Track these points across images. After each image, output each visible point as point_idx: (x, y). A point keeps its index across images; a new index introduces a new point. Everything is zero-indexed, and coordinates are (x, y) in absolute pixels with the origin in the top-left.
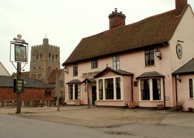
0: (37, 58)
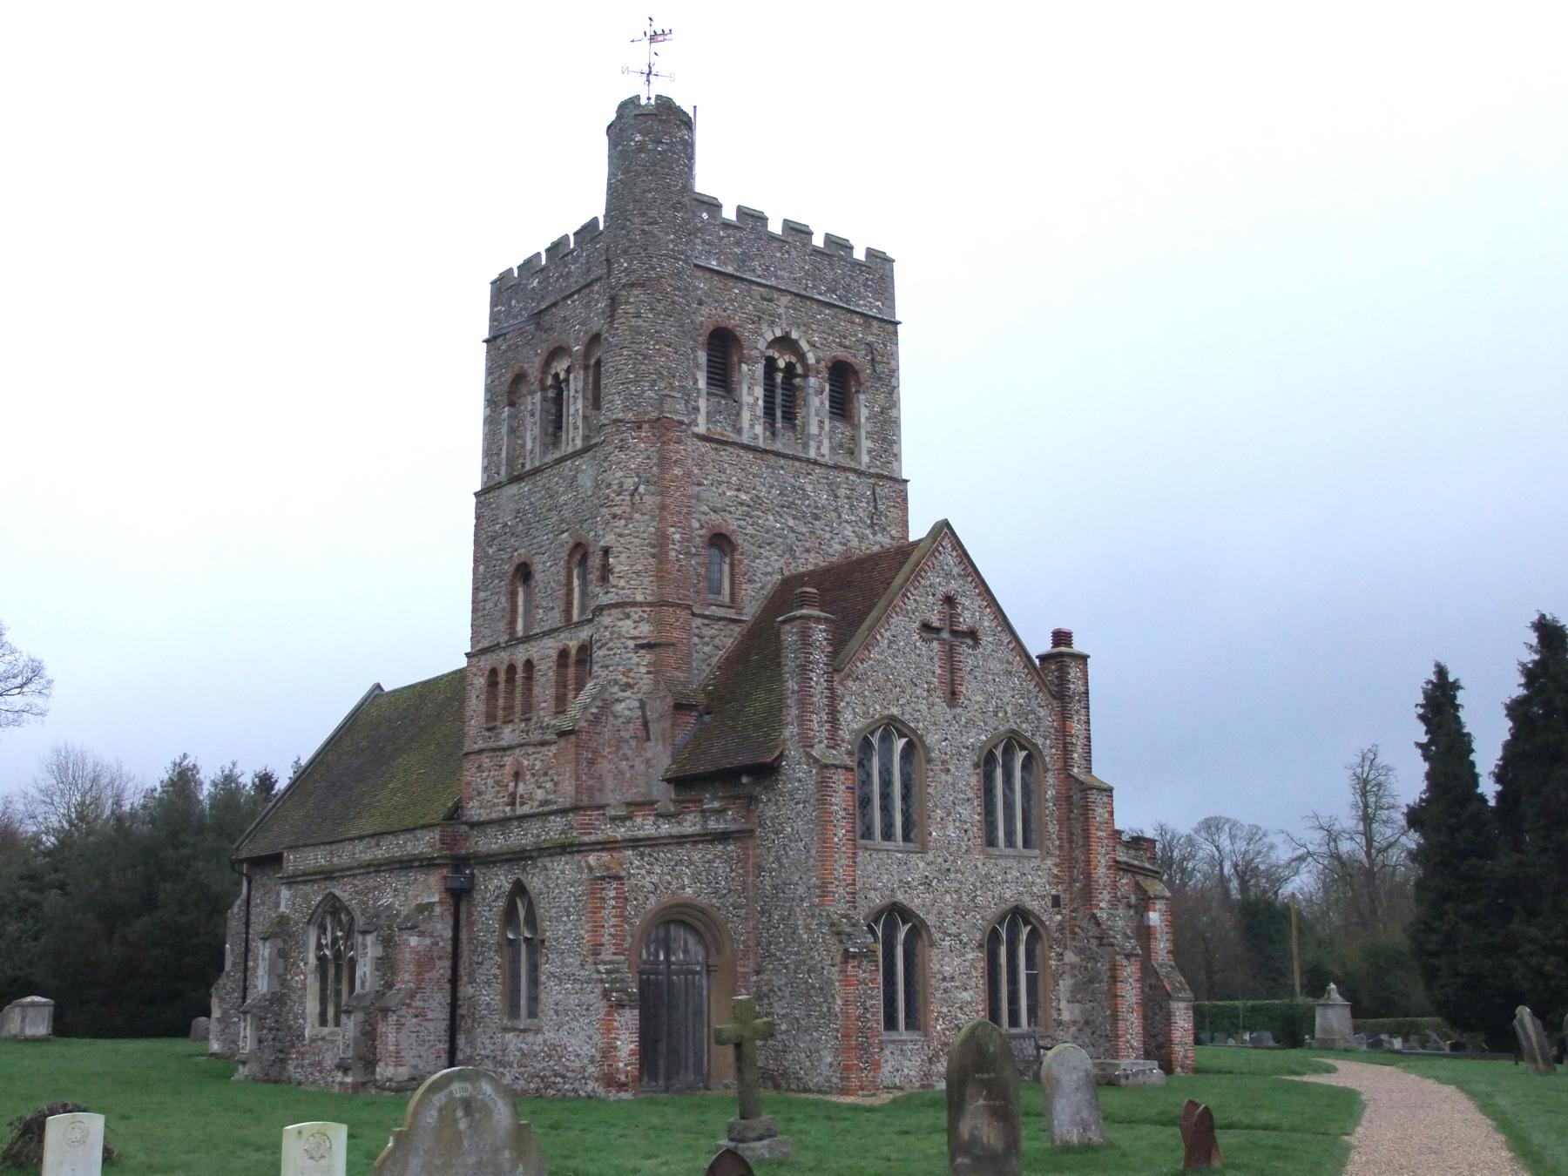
0: (555, 425)
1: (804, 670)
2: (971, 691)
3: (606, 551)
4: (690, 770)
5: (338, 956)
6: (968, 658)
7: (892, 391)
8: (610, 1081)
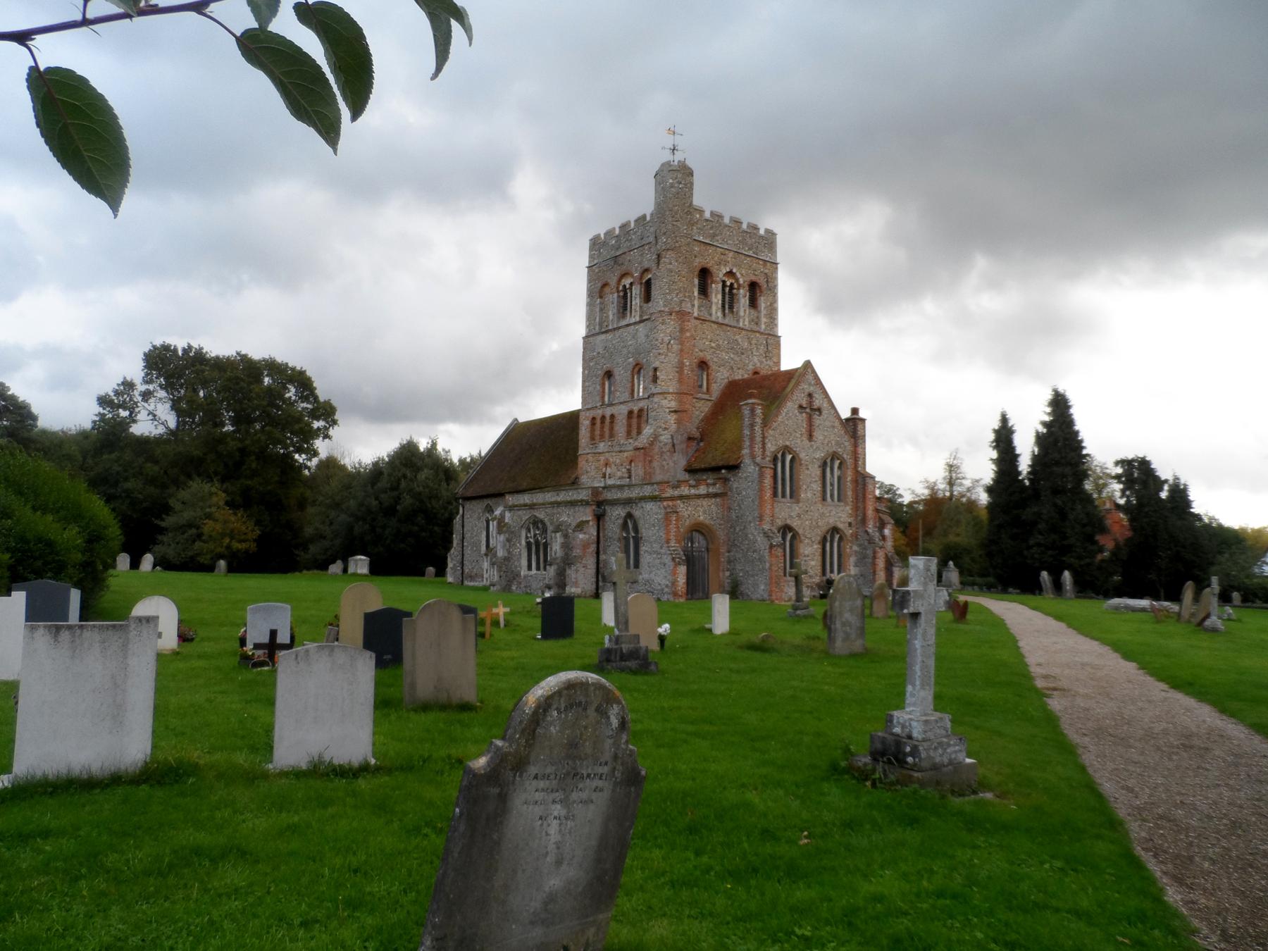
0: (624, 308)
1: (752, 426)
2: (818, 435)
3: (656, 369)
4: (696, 466)
5: (537, 543)
6: (817, 420)
7: (775, 295)
8: (675, 594)
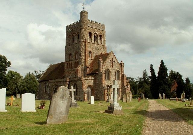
0: (74, 40)
6: (114, 63)
